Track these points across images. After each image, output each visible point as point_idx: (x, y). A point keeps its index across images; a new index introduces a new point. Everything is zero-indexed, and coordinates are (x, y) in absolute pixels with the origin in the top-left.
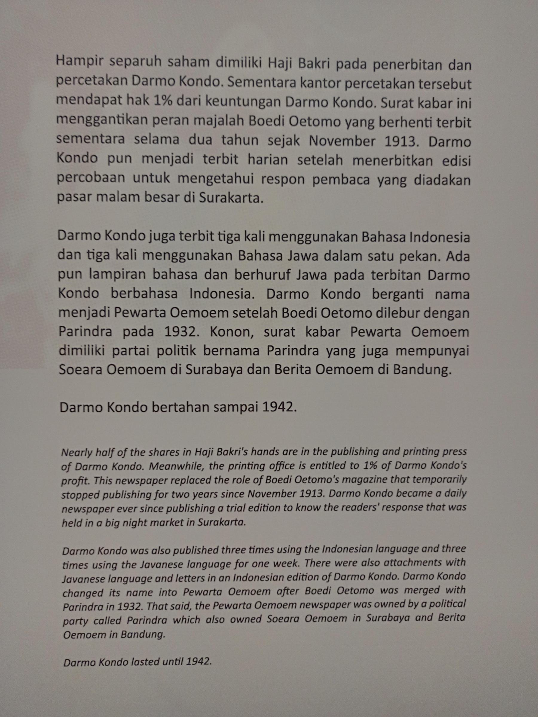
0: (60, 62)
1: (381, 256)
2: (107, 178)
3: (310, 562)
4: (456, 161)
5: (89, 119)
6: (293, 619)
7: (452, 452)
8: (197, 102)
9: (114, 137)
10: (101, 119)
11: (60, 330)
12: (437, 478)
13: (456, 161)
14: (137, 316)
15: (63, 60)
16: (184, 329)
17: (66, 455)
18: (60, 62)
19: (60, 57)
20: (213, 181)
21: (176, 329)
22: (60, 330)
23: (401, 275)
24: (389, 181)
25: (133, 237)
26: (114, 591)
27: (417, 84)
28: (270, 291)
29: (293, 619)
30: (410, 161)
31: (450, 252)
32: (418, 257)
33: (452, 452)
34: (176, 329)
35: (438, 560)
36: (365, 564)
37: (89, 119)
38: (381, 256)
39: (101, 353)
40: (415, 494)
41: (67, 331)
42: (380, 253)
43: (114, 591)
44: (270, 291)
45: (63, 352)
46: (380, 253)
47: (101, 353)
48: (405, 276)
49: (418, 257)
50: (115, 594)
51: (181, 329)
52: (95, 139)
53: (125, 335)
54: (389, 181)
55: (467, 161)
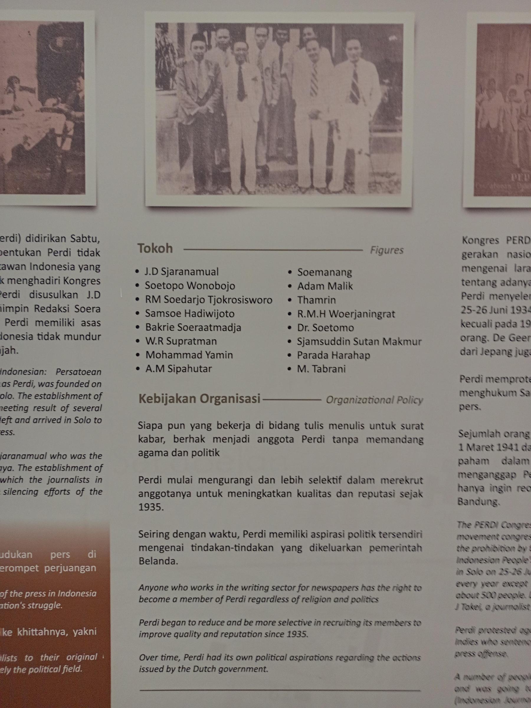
0: (335, 357)
1: (209, 327)
5: (221, 480)
7: (271, 623)
9: (176, 270)
11: (494, 338)
12: (263, 621)
14: (13, 269)
15: (337, 355)
16: (152, 505)
18: (335, 357)
19: (335, 353)
21: (147, 506)
22: (494, 338)
24: (289, 549)
25: (175, 286)
26: (228, 656)
30: (275, 494)
31: (142, 585)
33: (271, 623)
34: (147, 506)
37: (221, 480)
38: (209, 327)
39: (227, 302)
41: (303, 355)
42: (208, 325)
43: (228, 656)
46: (208, 325)
47: (227, 302)
50: (229, 658)
51: (150, 506)
53: (169, 428)
54: (289, 549)
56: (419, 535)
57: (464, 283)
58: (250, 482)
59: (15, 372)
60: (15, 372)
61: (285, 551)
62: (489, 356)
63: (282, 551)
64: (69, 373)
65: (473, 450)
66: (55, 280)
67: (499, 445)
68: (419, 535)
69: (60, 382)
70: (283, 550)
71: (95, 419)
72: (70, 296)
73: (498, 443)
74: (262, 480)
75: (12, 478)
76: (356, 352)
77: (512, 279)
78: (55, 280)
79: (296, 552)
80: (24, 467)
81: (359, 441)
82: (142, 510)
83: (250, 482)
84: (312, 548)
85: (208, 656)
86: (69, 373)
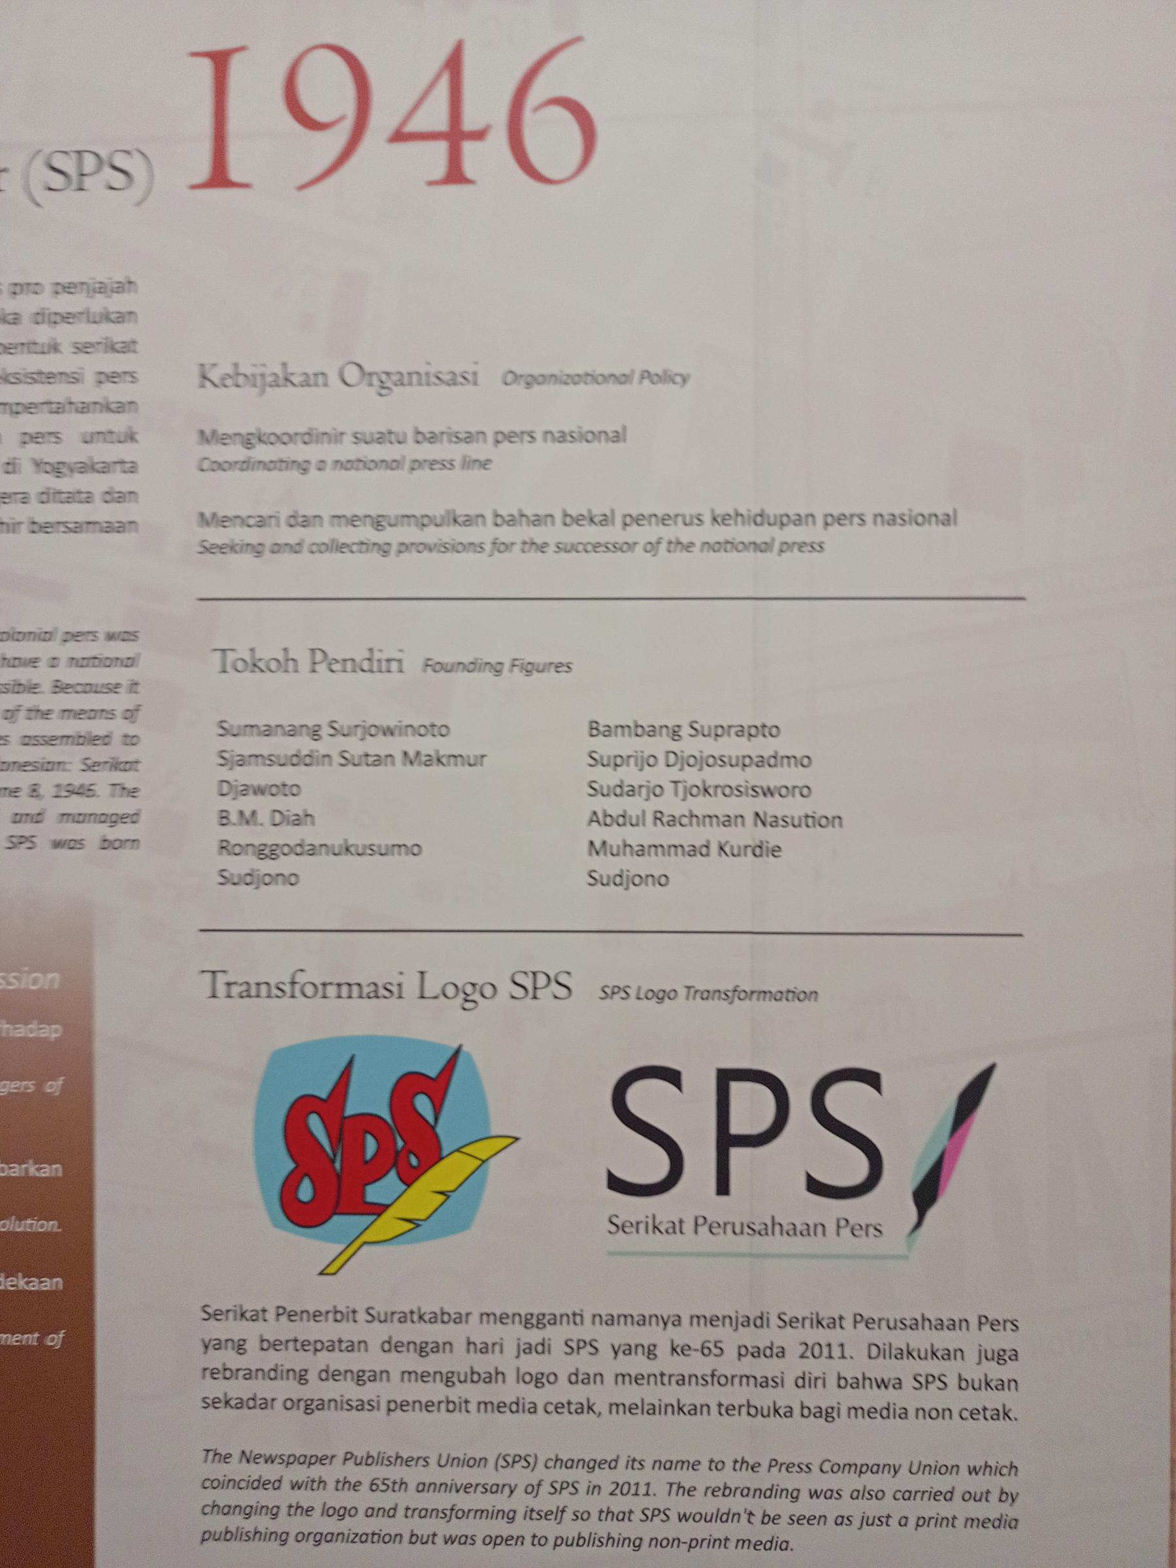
2: (942, 1325)
3: (675, 1487)
4: (1000, 1357)
6: (739, 1491)
8: (497, 1348)
10: (547, 1318)
13: (1000, 1357)
17: (248, 1461)
20: (544, 1380)
23: (351, 1315)
27: (714, 1409)
28: (735, 1087)
29: (739, 1491)
30: (416, 1317)
32: (227, 1402)
35: (638, 1458)
36: (856, 1495)
40: (907, 1495)
43: (532, 1511)
44: (735, 1087)
45: (386, 1347)
48: (344, 1346)
49: (227, 1402)
52: (652, 1379)
55: (778, 1381)
56: (820, 1382)
57: (723, 1411)
58: (835, 1415)
59: (387, 1539)
60: (387, 1539)
61: (620, 1354)
62: (310, 1354)
63: (613, 1354)
64: (480, 1489)
65: (602, 854)
66: (816, 1379)
67: (535, 997)
68: (820, 1382)
69: (456, 1508)
70: (616, 1353)
71: (534, 1536)
72: (948, 1355)
73: (215, 847)
74: (741, 1464)
75: (744, 512)
76: (867, 1375)
77: (581, 1371)
78: (816, 1379)
79: (645, 1359)
80: (679, 1487)
81: (786, 1352)
82: (214, 996)
83: (835, 1415)
84: (800, 1382)
85: (469, 1343)
86: (480, 1489)
